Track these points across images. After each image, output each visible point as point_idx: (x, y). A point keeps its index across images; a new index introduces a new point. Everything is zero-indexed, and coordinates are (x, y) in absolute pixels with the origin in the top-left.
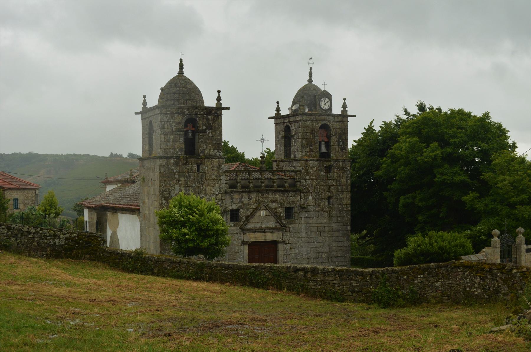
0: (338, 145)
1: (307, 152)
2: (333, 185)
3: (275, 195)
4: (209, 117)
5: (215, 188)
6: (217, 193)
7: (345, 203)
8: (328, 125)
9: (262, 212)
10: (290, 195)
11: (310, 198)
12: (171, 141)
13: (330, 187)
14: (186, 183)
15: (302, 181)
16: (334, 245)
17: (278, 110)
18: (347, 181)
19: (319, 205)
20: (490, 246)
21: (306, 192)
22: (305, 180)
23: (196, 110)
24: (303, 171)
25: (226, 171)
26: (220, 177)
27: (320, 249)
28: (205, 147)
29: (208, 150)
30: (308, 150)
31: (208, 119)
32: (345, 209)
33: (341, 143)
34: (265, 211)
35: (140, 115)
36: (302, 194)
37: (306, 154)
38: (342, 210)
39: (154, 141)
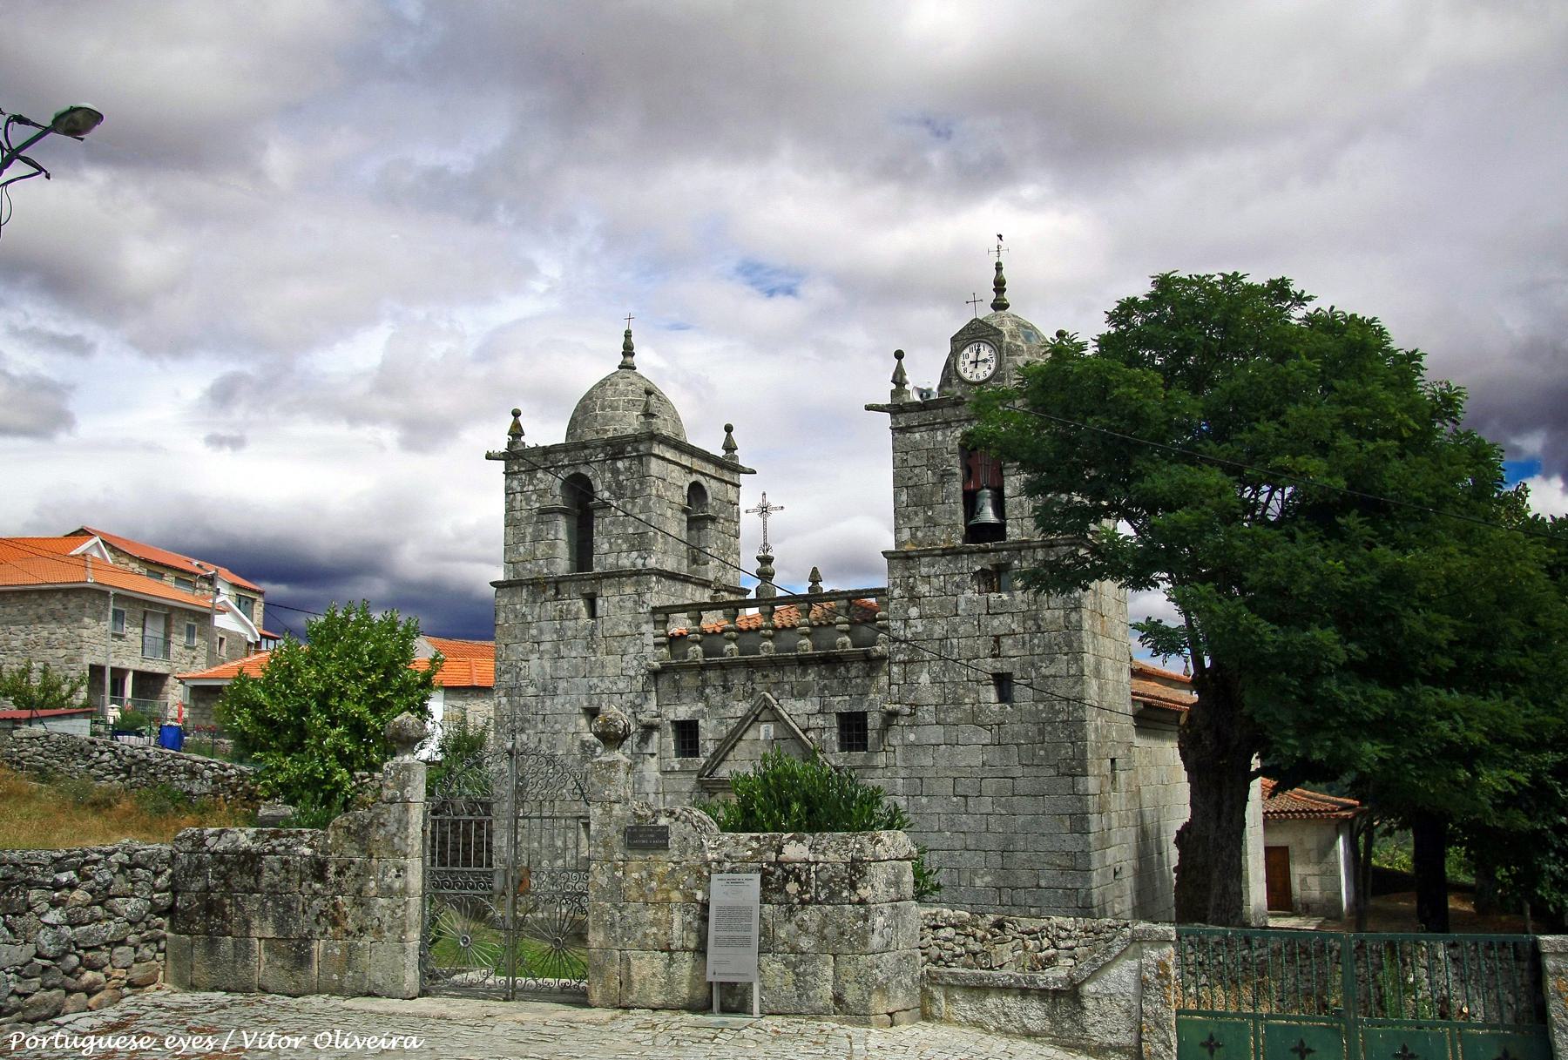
1: (917, 529)
2: (1013, 633)
3: (805, 673)
4: (620, 464)
5: (626, 658)
6: (632, 673)
9: (763, 727)
10: (853, 673)
11: (924, 678)
12: (528, 539)
13: (997, 639)
14: (556, 644)
17: (899, 379)
18: (1067, 617)
19: (958, 703)
21: (911, 661)
22: (906, 621)
24: (897, 592)
25: (655, 610)
26: (638, 626)
27: (967, 855)
28: (606, 546)
30: (921, 524)
31: (616, 472)
34: (771, 727)
35: (500, 465)
36: (895, 669)
37: (913, 536)
38: (1051, 722)
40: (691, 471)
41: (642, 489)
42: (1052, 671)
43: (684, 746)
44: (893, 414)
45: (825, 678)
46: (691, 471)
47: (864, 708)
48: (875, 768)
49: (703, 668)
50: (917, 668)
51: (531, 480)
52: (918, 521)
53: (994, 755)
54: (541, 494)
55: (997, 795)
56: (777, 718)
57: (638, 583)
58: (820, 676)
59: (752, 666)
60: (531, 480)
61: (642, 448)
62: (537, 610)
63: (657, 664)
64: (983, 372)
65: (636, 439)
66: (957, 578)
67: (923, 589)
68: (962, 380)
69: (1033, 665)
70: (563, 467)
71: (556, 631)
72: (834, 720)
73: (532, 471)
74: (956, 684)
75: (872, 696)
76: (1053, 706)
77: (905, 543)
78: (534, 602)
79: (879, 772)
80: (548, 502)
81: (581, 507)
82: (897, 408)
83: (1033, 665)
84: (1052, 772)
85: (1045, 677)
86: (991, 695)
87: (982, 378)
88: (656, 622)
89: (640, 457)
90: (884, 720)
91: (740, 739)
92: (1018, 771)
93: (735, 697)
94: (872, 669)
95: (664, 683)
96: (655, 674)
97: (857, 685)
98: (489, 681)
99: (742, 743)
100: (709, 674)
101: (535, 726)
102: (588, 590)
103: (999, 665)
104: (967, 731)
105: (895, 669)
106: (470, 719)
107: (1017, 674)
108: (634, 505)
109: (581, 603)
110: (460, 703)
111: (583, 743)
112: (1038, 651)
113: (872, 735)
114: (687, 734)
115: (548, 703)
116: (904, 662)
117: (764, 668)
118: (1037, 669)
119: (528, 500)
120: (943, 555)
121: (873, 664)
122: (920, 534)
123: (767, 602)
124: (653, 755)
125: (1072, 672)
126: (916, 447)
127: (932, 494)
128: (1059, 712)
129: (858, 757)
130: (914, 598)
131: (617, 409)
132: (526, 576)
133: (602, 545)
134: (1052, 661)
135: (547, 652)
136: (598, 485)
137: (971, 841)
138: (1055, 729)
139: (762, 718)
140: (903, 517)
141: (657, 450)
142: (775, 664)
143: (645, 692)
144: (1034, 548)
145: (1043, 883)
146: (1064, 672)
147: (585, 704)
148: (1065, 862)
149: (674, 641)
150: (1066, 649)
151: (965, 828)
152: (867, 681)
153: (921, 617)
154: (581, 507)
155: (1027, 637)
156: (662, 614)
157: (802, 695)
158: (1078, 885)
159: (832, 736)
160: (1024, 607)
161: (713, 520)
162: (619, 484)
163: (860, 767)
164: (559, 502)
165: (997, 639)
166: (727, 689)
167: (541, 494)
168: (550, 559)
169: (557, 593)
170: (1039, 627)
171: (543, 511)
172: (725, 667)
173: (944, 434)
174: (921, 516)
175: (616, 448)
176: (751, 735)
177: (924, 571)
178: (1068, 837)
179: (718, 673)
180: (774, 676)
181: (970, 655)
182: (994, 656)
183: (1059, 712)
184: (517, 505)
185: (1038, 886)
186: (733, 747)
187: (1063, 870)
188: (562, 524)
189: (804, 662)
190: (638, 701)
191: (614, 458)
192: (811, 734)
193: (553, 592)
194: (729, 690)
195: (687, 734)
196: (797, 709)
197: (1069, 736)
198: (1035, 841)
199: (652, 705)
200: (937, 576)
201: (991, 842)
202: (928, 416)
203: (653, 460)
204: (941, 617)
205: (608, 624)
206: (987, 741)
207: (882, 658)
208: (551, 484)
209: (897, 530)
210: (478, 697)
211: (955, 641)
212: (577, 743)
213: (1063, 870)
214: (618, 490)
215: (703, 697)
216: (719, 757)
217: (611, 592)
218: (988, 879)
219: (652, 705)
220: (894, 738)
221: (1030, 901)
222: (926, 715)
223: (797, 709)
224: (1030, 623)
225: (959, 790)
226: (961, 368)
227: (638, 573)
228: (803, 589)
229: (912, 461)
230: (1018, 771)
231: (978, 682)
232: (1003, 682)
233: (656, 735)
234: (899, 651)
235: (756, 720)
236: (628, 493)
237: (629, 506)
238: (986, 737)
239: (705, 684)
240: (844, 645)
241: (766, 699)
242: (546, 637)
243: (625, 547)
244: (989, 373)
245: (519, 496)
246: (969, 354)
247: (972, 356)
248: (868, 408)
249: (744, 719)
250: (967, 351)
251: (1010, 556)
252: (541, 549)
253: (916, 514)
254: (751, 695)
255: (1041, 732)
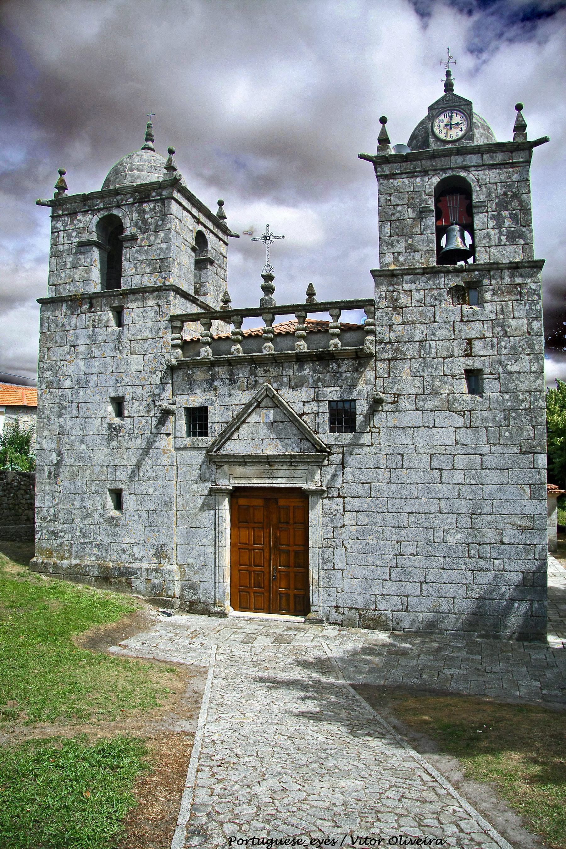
0: (499, 225)
1: (399, 254)
3: (301, 368)
5: (147, 357)
7: (523, 387)
8: (464, 179)
10: (344, 368)
12: (68, 266)
13: (470, 342)
15: (379, 329)
16: (488, 509)
18: (529, 325)
20: (330, 402)
21: (395, 359)
23: (119, 197)
25: (173, 318)
26: (158, 332)
27: (441, 516)
29: (139, 277)
32: (525, 405)
33: (507, 223)
36: (379, 364)
37: (396, 260)
39: (211, 234)
40: (199, 222)
41: (164, 224)
42: (515, 368)
43: (195, 427)
44: (375, 164)
45: (318, 372)
46: (199, 222)
47: (354, 395)
48: (362, 446)
49: (213, 364)
50: (400, 364)
51: (72, 221)
52: (401, 247)
53: (465, 436)
54: (80, 231)
55: (467, 470)
56: (277, 404)
57: (159, 297)
58: (315, 370)
59: (255, 363)
60: (72, 221)
61: (164, 193)
62: (74, 320)
63: (174, 362)
64: (455, 134)
65: (158, 186)
66: (435, 292)
67: (404, 300)
68: (438, 139)
69: (500, 363)
70: (99, 210)
71: (89, 337)
72: (325, 407)
73: (73, 214)
74: (434, 377)
75: (359, 387)
76: (517, 397)
77: (388, 265)
78: (72, 314)
79: (366, 449)
80: (85, 237)
81: (113, 242)
82: (379, 162)
83: (500, 363)
84: (515, 450)
85: (510, 373)
86: (463, 386)
87: (455, 138)
88: (173, 328)
89: (163, 200)
90: (371, 407)
91: (244, 422)
92: (486, 449)
93: (239, 388)
94: (360, 365)
95: (179, 376)
96: (172, 369)
97: (347, 378)
98: (34, 403)
99: (245, 425)
100: (218, 369)
101: (71, 412)
102: (116, 304)
103: (470, 362)
104: (442, 418)
105: (379, 364)
106: (21, 426)
107: (487, 370)
108: (156, 237)
109: (111, 314)
110: (14, 416)
111: (110, 426)
112: (504, 352)
113: (360, 419)
114: (198, 420)
115: (81, 394)
116: (389, 360)
117: (266, 364)
118: (504, 366)
119: (69, 236)
120: (423, 274)
121: (361, 358)
122: (401, 258)
123: (268, 311)
124: (168, 435)
125: (533, 369)
126: (398, 191)
127: (412, 227)
128: (523, 401)
129: (347, 437)
130: (397, 308)
131: (142, 171)
132: (65, 294)
133: (127, 267)
134: (516, 360)
135: (82, 353)
136: (127, 223)
137: (444, 506)
138: (519, 415)
139: (263, 404)
140: (387, 244)
141: (177, 195)
142: (275, 360)
143: (163, 384)
144: (502, 270)
145: (506, 540)
146: (527, 369)
147: (113, 394)
148: (525, 523)
149: (186, 345)
150: (528, 351)
151: (439, 495)
152: (356, 375)
153: (403, 323)
154: (113, 242)
155: (495, 340)
156: (178, 322)
157: (299, 385)
158: (536, 541)
159: (324, 420)
160: (493, 316)
161: (211, 262)
162: (145, 222)
163: (348, 445)
164: (94, 237)
165: (470, 342)
166: (233, 381)
167: (80, 231)
168: (86, 281)
169: (91, 306)
170: (506, 332)
171: (81, 244)
172: (231, 363)
173: (422, 180)
174: (403, 244)
175: (143, 194)
176: (254, 418)
177: (406, 286)
178: (528, 503)
179: (225, 368)
180: (273, 371)
181: (445, 354)
182: (467, 355)
183: (523, 401)
184: (61, 240)
185: (502, 542)
186: (238, 428)
187: (523, 530)
188: (96, 254)
189: (301, 359)
190: (157, 391)
191: (141, 201)
192: (305, 418)
193: (87, 306)
194: (235, 382)
195: (198, 420)
196: (295, 399)
197: (531, 421)
198: (499, 506)
199: (168, 394)
200: (417, 290)
201: (462, 506)
202: (409, 166)
203: (173, 202)
204: (421, 323)
205: (133, 330)
206: (461, 425)
207: (370, 356)
208: (90, 222)
209: (382, 254)
210: (27, 413)
211: (433, 343)
212: (105, 425)
213: (523, 530)
214: (144, 227)
215: (211, 387)
216: (226, 435)
217: (135, 305)
218: (459, 536)
219: (168, 394)
220: (378, 420)
221: (494, 555)
222: (406, 403)
223: (295, 399)
224: (498, 329)
225: (435, 464)
226: (436, 130)
227: (159, 289)
228: (302, 300)
229: (395, 201)
230: (486, 449)
231: (453, 376)
232: (473, 377)
233: (172, 418)
234: (383, 350)
235: (258, 406)
236: (152, 228)
237: (152, 238)
238: (459, 421)
239: (214, 377)
240: (336, 345)
241: (267, 389)
242: (81, 341)
243: (148, 270)
244: (461, 134)
245: (62, 234)
246: (443, 119)
247: (446, 121)
248: (361, 157)
249: (248, 406)
250: (441, 117)
251: (480, 276)
252: (79, 273)
253: (398, 242)
254: (254, 387)
255: (506, 418)
